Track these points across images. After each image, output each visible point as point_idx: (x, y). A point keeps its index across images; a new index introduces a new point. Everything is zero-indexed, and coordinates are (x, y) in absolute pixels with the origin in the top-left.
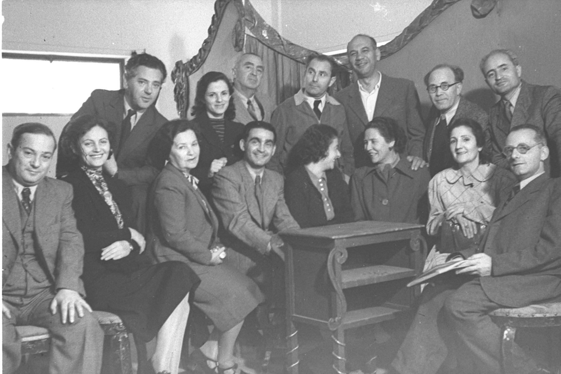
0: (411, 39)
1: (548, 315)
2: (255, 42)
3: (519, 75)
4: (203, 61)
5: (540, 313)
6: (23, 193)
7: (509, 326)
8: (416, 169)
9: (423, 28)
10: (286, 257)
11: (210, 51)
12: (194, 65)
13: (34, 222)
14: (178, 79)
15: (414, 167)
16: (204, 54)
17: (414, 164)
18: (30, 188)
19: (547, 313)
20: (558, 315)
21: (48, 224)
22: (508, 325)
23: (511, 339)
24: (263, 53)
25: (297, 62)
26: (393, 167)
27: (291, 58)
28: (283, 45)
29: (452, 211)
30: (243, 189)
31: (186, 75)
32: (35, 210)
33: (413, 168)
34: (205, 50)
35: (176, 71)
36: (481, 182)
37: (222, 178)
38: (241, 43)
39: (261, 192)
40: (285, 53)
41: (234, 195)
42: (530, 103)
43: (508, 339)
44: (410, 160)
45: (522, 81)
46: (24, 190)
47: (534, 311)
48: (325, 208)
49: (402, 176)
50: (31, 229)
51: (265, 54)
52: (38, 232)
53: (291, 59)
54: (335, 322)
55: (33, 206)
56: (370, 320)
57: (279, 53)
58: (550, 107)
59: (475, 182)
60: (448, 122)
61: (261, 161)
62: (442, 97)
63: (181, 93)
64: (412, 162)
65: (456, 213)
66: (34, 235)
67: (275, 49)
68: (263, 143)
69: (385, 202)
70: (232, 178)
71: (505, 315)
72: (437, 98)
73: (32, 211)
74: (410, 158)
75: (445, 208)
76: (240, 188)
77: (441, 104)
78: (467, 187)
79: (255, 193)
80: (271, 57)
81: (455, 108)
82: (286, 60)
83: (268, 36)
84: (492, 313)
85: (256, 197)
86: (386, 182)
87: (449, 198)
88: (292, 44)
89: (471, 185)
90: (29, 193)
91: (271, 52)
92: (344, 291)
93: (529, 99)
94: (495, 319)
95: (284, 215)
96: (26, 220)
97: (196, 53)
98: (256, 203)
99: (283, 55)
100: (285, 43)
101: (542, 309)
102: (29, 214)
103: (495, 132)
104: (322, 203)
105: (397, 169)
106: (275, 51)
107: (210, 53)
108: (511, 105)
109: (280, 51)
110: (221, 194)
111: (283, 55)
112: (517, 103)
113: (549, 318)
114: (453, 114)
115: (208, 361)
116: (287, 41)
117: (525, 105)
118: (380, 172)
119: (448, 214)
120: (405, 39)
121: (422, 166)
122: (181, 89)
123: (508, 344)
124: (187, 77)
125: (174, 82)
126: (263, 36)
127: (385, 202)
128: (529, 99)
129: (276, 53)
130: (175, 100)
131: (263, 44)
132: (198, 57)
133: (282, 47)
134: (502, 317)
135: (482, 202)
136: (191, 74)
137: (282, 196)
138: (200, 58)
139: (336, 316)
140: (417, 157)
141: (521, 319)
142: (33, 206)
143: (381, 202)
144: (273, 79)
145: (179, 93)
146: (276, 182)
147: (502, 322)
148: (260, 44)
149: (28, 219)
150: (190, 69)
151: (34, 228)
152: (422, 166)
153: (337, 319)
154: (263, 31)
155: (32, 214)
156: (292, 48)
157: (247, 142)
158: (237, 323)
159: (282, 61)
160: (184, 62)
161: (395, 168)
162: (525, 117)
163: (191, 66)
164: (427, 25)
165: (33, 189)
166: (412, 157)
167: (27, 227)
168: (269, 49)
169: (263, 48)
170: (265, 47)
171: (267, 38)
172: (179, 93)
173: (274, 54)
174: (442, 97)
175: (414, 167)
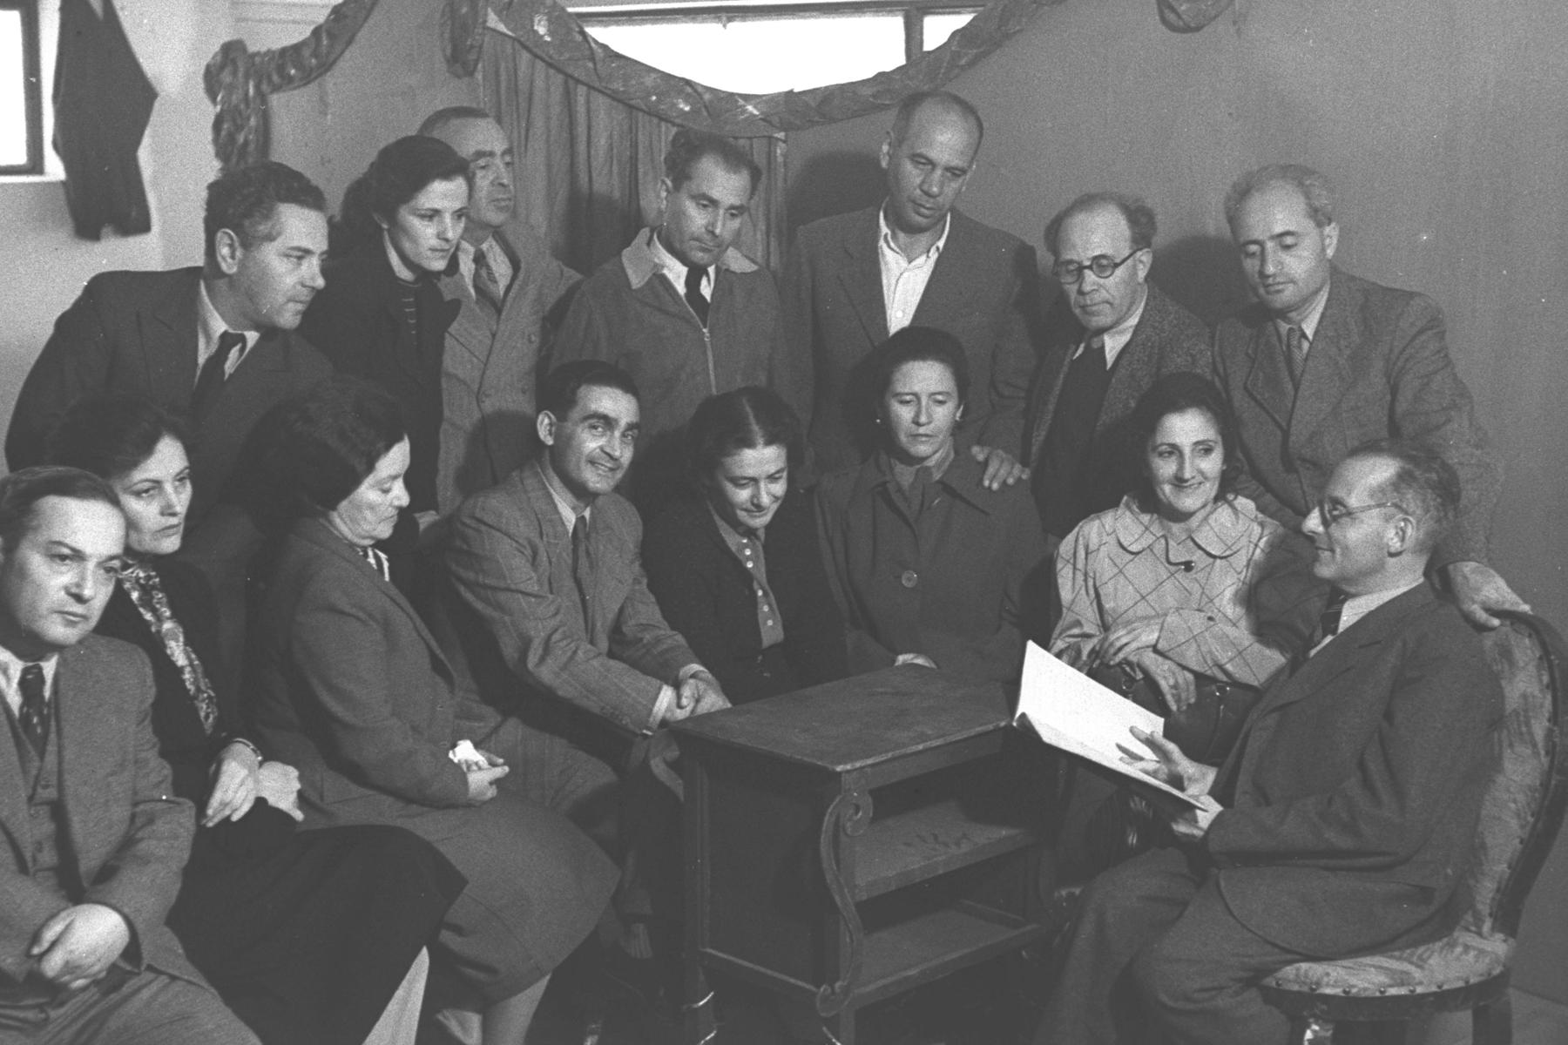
0: (972, 63)
1: (1419, 990)
2: (509, 51)
4: (326, 66)
5: (1402, 984)
6: (23, 684)
8: (995, 486)
9: (1008, 36)
11: (349, 42)
13: (60, 773)
16: (331, 46)
17: (991, 470)
18: (42, 664)
19: (1421, 983)
20: (1445, 987)
22: (1314, 1016)
24: (532, 82)
25: (631, 107)
27: (614, 97)
28: (592, 58)
29: (1124, 640)
31: (257, 87)
33: (986, 483)
34: (332, 37)
35: (222, 67)
36: (1214, 557)
37: (483, 528)
38: (472, 56)
39: (591, 567)
40: (597, 85)
44: (981, 457)
46: (25, 672)
47: (1383, 979)
48: (760, 616)
50: (52, 793)
51: (539, 83)
52: (71, 805)
53: (614, 99)
54: (833, 992)
55: (53, 723)
57: (578, 81)
59: (1197, 557)
60: (1110, 356)
61: (595, 480)
63: (241, 139)
64: (985, 464)
65: (1134, 645)
66: (58, 811)
67: (570, 70)
69: (909, 579)
70: (513, 530)
73: (53, 736)
74: (979, 453)
75: (1105, 627)
76: (535, 554)
77: (1093, 314)
78: (1173, 569)
79: (575, 570)
80: (557, 95)
81: (1133, 321)
82: (600, 102)
83: (550, 33)
84: (1270, 982)
87: (1119, 598)
89: (1188, 566)
90: (41, 679)
91: (560, 77)
92: (860, 906)
96: (34, 772)
97: (300, 34)
98: (576, 597)
101: (1407, 973)
102: (42, 755)
104: (753, 602)
105: (945, 487)
106: (568, 76)
107: (352, 48)
108: (1304, 336)
109: (583, 78)
113: (1423, 996)
114: (1126, 338)
117: (1343, 343)
118: (900, 490)
119: (1112, 651)
122: (239, 128)
124: (262, 97)
125: (214, 101)
126: (536, 32)
127: (909, 579)
129: (571, 82)
131: (536, 56)
132: (306, 52)
133: (590, 65)
135: (1210, 619)
136: (276, 89)
137: (636, 567)
138: (315, 54)
139: (837, 979)
140: (1000, 452)
143: (899, 577)
145: (232, 137)
148: (526, 56)
149: (40, 769)
150: (275, 78)
152: (1011, 481)
153: (838, 985)
154: (536, 20)
155: (51, 748)
158: (543, 976)
159: (588, 102)
160: (252, 49)
161: (940, 482)
163: (281, 69)
164: (1020, 31)
165: (49, 667)
166: (986, 450)
167: (40, 790)
168: (552, 71)
169: (547, 77)
170: (540, 65)
171: (548, 39)
173: (566, 82)
174: (1097, 297)
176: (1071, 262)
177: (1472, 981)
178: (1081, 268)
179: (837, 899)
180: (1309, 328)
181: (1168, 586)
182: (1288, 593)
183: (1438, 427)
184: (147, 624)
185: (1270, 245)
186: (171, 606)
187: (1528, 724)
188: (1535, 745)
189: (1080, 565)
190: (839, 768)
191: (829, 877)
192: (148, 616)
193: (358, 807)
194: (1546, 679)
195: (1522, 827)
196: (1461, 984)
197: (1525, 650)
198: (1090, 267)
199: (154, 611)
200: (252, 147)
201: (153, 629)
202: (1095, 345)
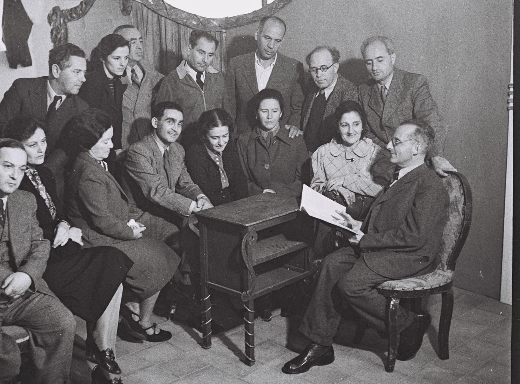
1: (425, 288)
2: (140, 7)
3: (393, 63)
5: (420, 287)
7: (394, 298)
8: (293, 137)
10: (201, 232)
11: (92, 6)
12: (74, 15)
14: (55, 23)
15: (292, 135)
16: (86, 7)
17: (291, 132)
19: (426, 286)
20: (433, 287)
21: (21, 232)
22: (393, 297)
23: (396, 308)
25: (178, 23)
26: (275, 134)
27: (173, 20)
28: (166, 9)
29: (333, 184)
30: (154, 162)
31: (64, 20)
32: (8, 220)
33: (290, 136)
37: (136, 154)
38: (129, 9)
39: (169, 165)
40: (168, 17)
41: (148, 167)
42: (402, 89)
43: (394, 308)
44: (288, 128)
45: (395, 69)
49: (281, 142)
50: (6, 239)
51: (150, 17)
52: (12, 242)
55: (6, 217)
56: (274, 287)
57: (162, 16)
58: (419, 94)
61: (171, 138)
62: (322, 78)
63: (59, 37)
64: (289, 130)
65: (336, 185)
67: (159, 13)
68: (176, 124)
69: (267, 166)
70: (145, 154)
71: (391, 289)
72: (317, 79)
73: (6, 221)
74: (287, 127)
76: (152, 161)
77: (321, 83)
78: (347, 161)
79: (164, 166)
80: (155, 19)
81: (334, 85)
82: (169, 22)
85: (166, 170)
86: (267, 147)
88: (174, 8)
89: (352, 160)
91: (156, 15)
93: (401, 85)
94: (382, 292)
95: (186, 183)
99: (165, 18)
100: (168, 7)
103: (366, 110)
107: (92, 8)
108: (386, 88)
109: (163, 15)
110: (137, 168)
111: (165, 18)
112: (390, 87)
113: (426, 290)
114: (331, 90)
115: (147, 331)
116: (170, 5)
117: (398, 90)
118: (263, 139)
119: (329, 187)
120: (276, 7)
121: (297, 135)
122: (58, 33)
123: (394, 312)
124: (65, 23)
125: (51, 25)
127: (267, 166)
128: (401, 85)
130: (52, 41)
131: (149, 8)
132: (78, 9)
134: (389, 290)
138: (81, 10)
141: (405, 292)
142: (6, 217)
144: (157, 40)
145: (56, 36)
146: (180, 152)
147: (390, 294)
148: (145, 8)
150: (69, 17)
151: (9, 237)
152: (297, 135)
153: (248, 291)
155: (6, 225)
156: (174, 11)
157: (161, 121)
159: (165, 22)
161: (276, 136)
162: (398, 101)
163: (71, 15)
166: (290, 126)
167: (3, 238)
169: (152, 15)
171: (152, 3)
172: (56, 36)
174: (322, 78)
175: (292, 135)
176: (314, 67)
177: (441, 285)
178: (317, 69)
179: (247, 265)
180: (388, 86)
181: (346, 166)
182: (383, 168)
183: (427, 116)
184: (34, 186)
185: (375, 61)
186: (41, 180)
187: (457, 206)
188: (459, 212)
189: (319, 160)
190: (247, 225)
191: (244, 259)
192: (34, 183)
193: (100, 241)
194: (462, 192)
195: (456, 237)
196: (438, 286)
197: (455, 183)
198: (320, 69)
199: (36, 182)
200: (62, 39)
201: (36, 188)
202: (322, 93)
